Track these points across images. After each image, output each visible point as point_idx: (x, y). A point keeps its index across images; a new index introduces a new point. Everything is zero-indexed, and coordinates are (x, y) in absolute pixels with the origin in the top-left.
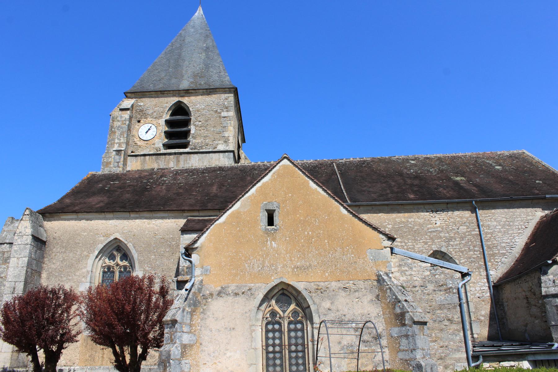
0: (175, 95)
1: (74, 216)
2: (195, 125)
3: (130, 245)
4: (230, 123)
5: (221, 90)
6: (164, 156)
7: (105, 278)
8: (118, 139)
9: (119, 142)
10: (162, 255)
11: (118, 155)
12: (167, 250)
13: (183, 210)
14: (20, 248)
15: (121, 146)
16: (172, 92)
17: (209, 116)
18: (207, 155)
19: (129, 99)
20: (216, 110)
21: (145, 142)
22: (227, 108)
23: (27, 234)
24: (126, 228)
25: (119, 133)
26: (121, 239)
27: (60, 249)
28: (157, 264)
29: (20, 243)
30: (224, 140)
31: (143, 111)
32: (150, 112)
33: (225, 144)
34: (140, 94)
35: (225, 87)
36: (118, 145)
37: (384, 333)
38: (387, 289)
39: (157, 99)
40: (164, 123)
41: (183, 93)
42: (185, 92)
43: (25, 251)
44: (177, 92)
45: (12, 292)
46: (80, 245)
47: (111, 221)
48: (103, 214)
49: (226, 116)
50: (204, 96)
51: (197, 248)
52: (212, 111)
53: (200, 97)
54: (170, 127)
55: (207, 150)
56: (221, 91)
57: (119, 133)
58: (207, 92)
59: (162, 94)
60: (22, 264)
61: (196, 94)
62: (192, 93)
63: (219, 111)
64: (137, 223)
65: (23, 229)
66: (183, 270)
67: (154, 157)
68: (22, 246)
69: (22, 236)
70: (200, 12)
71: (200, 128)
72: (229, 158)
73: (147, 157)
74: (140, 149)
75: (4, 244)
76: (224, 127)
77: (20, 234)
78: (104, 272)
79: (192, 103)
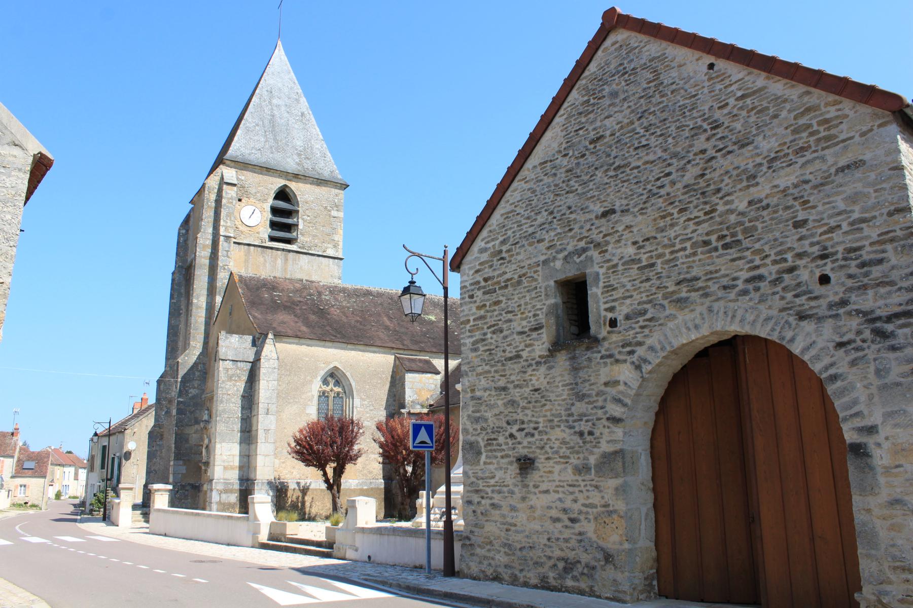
1: (296, 340)
2: (303, 219)
32: (253, 191)
39: (261, 176)
40: (269, 209)
47: (330, 350)
53: (309, 186)
67: (259, 249)
73: (252, 248)
78: (320, 396)
79: (300, 191)
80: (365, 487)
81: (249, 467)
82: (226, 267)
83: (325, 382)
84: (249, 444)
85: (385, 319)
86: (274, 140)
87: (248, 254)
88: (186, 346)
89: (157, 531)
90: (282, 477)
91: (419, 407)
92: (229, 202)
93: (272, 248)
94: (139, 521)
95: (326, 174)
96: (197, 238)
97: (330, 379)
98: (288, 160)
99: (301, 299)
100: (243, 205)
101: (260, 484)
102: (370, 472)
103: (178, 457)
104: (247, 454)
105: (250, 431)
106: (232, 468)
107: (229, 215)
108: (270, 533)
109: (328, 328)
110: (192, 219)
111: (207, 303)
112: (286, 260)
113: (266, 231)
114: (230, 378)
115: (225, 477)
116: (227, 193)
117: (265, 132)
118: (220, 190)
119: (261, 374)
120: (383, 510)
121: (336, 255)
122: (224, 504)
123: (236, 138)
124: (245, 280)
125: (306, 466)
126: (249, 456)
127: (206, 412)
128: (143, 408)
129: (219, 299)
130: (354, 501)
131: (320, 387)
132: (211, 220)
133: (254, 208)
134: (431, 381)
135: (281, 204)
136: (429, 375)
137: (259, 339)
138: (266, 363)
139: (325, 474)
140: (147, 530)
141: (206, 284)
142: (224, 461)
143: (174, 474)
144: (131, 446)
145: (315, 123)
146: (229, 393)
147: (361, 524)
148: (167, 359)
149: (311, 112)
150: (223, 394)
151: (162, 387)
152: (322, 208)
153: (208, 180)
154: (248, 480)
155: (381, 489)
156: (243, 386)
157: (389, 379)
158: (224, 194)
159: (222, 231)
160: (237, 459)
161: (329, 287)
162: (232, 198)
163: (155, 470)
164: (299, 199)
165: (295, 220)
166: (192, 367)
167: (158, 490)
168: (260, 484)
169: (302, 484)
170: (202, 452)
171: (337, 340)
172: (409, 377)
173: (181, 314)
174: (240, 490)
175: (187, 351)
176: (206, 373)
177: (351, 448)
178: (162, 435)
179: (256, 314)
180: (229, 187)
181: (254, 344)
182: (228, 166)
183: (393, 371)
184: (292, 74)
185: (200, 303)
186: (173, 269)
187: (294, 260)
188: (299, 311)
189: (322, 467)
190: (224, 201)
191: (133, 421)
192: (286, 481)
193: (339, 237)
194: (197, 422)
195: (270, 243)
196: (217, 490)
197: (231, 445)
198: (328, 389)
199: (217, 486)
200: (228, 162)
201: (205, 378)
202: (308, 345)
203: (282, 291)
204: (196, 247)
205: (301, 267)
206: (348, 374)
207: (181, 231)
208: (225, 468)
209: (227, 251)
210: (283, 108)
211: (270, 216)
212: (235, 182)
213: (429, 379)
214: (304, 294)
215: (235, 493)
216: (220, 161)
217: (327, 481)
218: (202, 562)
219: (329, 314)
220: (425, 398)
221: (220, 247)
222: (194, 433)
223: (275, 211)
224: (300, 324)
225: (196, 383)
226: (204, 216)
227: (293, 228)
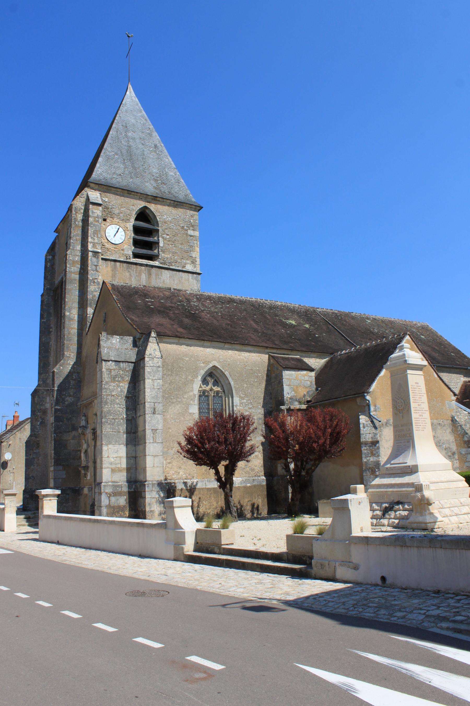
0: (141, 199)
1: (176, 340)
2: (163, 238)
3: (227, 374)
4: (197, 243)
5: (187, 205)
6: (135, 266)
7: (201, 401)
8: (92, 238)
9: (93, 241)
10: (252, 385)
11: (95, 257)
12: (256, 380)
13: (266, 347)
15: (96, 246)
16: (139, 195)
17: (176, 231)
18: (177, 273)
19: (92, 190)
20: (183, 226)
21: (114, 245)
22: (193, 226)
23: (157, 357)
24: (221, 357)
25: (92, 231)
26: (219, 367)
27: (167, 371)
28: (249, 392)
29: (152, 365)
30: (192, 260)
31: (109, 208)
32: (116, 211)
33: (193, 264)
34: (105, 187)
35: (191, 204)
36: (92, 245)
37: (456, 452)
38: (458, 426)
39: (122, 198)
40: (132, 228)
42: (152, 198)
43: (158, 373)
44: (145, 196)
45: (153, 413)
46: (185, 369)
47: (208, 350)
48: (203, 341)
49: (193, 235)
50: (171, 208)
51: (370, 392)
52: (179, 226)
55: (177, 268)
56: (188, 207)
57: (92, 231)
58: (174, 204)
59: (128, 194)
60: (158, 386)
61: (163, 203)
62: (159, 201)
63: (185, 228)
64: (230, 354)
65: (153, 352)
66: (287, 400)
67: (125, 265)
68: (155, 369)
69: (153, 358)
70: (130, 93)
71: (168, 242)
72: (198, 281)
73: (118, 264)
74: (109, 252)
75: (109, 361)
76: (191, 246)
77: (151, 356)
78: (200, 396)
79: (159, 212)
80: (249, 485)
81: (136, 469)
82: (96, 281)
83: (205, 381)
84: (135, 445)
85: (252, 322)
86: (132, 167)
87: (114, 270)
88: (59, 356)
89: (48, 538)
90: (169, 478)
91: (297, 403)
92: (95, 221)
93: (136, 264)
94: (24, 525)
95: (181, 197)
96: (66, 255)
97: (209, 379)
98: (147, 184)
99: (173, 305)
100: (108, 224)
101: (150, 486)
102: (253, 470)
103: (58, 462)
104: (134, 455)
105: (136, 432)
106: (120, 470)
107: (96, 232)
108: (196, 543)
109: (202, 329)
110: (57, 246)
111: (79, 315)
112: (150, 274)
113: (129, 249)
114: (113, 379)
115: (113, 480)
116: (93, 212)
117: (124, 160)
118: (86, 211)
119: (146, 373)
120: (266, 507)
122: (114, 507)
123: (98, 165)
124: (118, 288)
125: (197, 465)
126: (135, 457)
127: (83, 418)
128: (15, 424)
129: (90, 311)
130: (346, 500)
131: (200, 387)
132: (79, 238)
133: (118, 227)
134: (306, 378)
135: (142, 224)
136: (305, 372)
137: (140, 339)
138: (150, 362)
139: (217, 473)
140: (36, 536)
141: (77, 297)
142: (111, 464)
143: (55, 479)
144: (7, 456)
145: (167, 154)
146: (113, 393)
147: (356, 532)
148: (40, 374)
149: (163, 145)
150: (107, 395)
151: (36, 399)
152: (179, 228)
153: (75, 202)
154: (136, 481)
155: (263, 486)
156: (127, 387)
157: (265, 378)
158: (90, 214)
159: (90, 247)
160: (124, 461)
161: (196, 295)
162: (98, 217)
163: (33, 477)
164: (158, 219)
165: (156, 238)
166: (68, 376)
167: (47, 496)
168: (150, 486)
169: (189, 484)
170: (80, 457)
171: (216, 340)
172: (287, 375)
173: (51, 332)
174: (129, 493)
175: (62, 361)
176: (80, 382)
177: (243, 447)
178: (38, 444)
179: (133, 317)
180: (95, 207)
181: (135, 344)
182: (92, 188)
183: (268, 370)
184: (144, 112)
185: (72, 315)
186: (42, 291)
187: (157, 275)
188: (172, 315)
189: (214, 465)
190: (91, 220)
191: (8, 435)
192: (173, 481)
193: (196, 254)
194: (74, 428)
195: (134, 259)
196: (106, 493)
197: (117, 447)
198: (208, 388)
199: (106, 489)
200: (92, 185)
201: (80, 386)
202: (187, 345)
203: (153, 297)
204: (66, 263)
205: (164, 281)
206: (227, 373)
207: (48, 257)
208: (113, 471)
209: (96, 266)
210: (138, 141)
211: (133, 235)
212: (100, 202)
213: (304, 376)
214: (175, 301)
215: (124, 495)
216: (85, 184)
217: (219, 479)
218: (143, 594)
219: (200, 318)
220: (302, 394)
221: (89, 262)
222: (72, 439)
223: (136, 230)
224: (175, 326)
225: (72, 392)
226: (72, 235)
227: (154, 246)
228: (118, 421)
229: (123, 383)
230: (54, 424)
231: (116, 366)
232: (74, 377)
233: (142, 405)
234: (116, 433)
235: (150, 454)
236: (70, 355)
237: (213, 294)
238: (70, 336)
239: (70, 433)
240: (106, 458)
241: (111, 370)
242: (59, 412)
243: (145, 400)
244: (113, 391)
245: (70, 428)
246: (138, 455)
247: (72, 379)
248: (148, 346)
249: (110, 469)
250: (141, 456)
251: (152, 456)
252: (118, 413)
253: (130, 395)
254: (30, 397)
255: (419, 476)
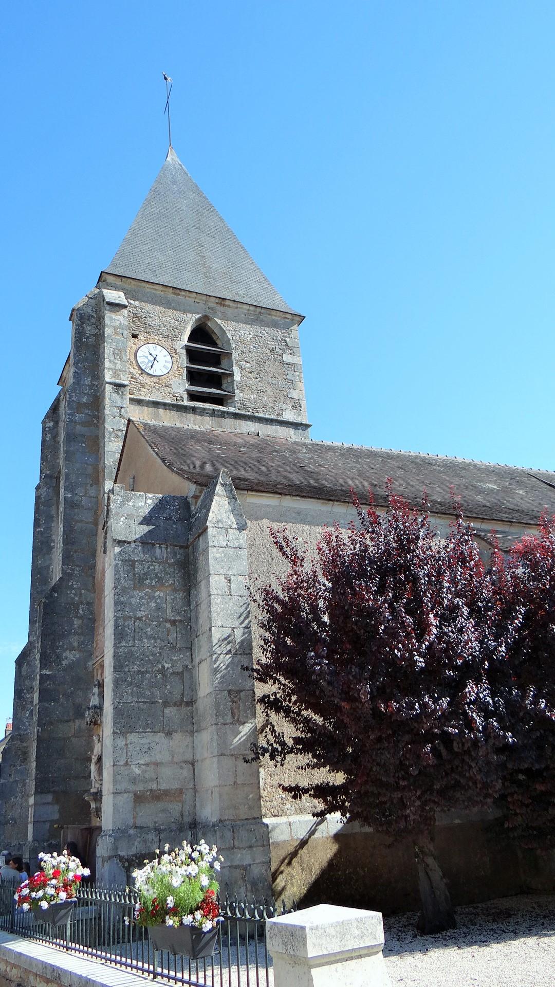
4: (298, 376)
8: (110, 361)
9: (112, 367)
14: (225, 555)
15: (119, 375)
16: (194, 295)
41: (213, 303)
42: (217, 301)
44: (204, 298)
54: (189, 363)
59: (175, 294)
68: (231, 552)
77: (220, 525)
80: (457, 821)
81: (195, 791)
84: (192, 733)
104: (189, 757)
113: (181, 386)
115: (139, 822)
116: (111, 318)
121: (299, 420)
146: (140, 614)
151: (24, 668)
163: (13, 819)
176: (93, 621)
207: (48, 425)
221: (107, 401)
223: (192, 355)
225: (74, 641)
228: (151, 677)
229: (162, 591)
230: (38, 707)
231: (144, 553)
232: (80, 611)
233: (206, 635)
234: (144, 706)
235: (224, 752)
236: (73, 570)
237: (337, 444)
238: (72, 536)
239: (71, 724)
240: (122, 768)
241: (134, 562)
242: (48, 682)
243: (210, 623)
244: (139, 607)
245: (71, 714)
246: (198, 757)
247: (77, 617)
248: (214, 502)
249: (132, 795)
250: (206, 759)
251: (232, 755)
252: (151, 658)
253: (178, 618)
254: (14, 665)
255: (114, 822)
